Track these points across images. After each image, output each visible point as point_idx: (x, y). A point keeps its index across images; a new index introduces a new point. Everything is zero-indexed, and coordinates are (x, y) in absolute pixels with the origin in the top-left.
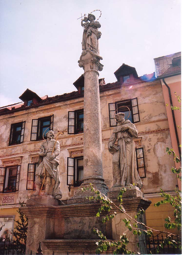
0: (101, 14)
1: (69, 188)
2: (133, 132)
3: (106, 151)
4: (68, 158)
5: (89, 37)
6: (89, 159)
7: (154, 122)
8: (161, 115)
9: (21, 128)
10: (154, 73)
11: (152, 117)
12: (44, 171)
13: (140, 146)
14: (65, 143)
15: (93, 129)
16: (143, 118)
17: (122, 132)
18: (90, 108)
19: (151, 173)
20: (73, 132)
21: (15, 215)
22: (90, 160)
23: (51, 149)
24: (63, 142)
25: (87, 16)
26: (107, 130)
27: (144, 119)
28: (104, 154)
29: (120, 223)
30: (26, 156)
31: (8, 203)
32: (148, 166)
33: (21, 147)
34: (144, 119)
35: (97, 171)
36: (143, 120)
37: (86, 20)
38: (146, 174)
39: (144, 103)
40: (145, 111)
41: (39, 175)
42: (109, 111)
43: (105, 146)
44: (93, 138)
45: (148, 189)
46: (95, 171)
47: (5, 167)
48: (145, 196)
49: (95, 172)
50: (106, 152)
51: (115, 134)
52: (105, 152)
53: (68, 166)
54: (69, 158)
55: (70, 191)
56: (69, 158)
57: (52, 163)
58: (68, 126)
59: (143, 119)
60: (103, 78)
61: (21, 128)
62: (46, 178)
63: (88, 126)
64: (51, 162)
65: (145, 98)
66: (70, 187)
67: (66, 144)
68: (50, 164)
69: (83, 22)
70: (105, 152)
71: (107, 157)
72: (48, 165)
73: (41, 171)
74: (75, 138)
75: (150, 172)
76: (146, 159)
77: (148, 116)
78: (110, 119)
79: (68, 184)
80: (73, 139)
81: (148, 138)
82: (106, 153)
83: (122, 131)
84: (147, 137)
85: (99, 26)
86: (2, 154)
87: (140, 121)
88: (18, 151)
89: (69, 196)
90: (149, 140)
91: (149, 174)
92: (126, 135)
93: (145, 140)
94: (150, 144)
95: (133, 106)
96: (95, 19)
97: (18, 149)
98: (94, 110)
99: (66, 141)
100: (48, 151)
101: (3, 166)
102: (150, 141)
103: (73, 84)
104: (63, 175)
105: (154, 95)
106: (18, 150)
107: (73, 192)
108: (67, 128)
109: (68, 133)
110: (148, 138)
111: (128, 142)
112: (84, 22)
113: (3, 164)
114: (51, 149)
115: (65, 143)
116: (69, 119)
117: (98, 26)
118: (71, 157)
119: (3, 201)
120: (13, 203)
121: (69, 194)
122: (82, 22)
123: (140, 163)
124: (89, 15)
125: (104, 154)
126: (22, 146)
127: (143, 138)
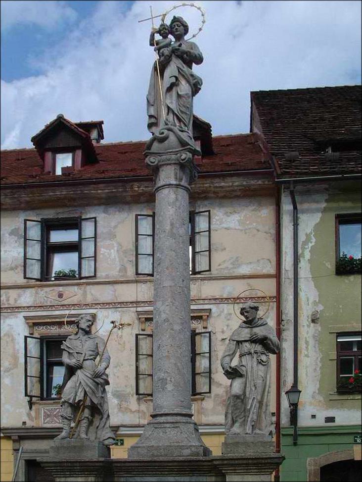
0: (204, 22)
1: (28, 402)
2: (273, 344)
4: (26, 337)
5: (174, 89)
6: (169, 379)
7: (243, 277)
8: (262, 262)
10: (191, 69)
11: (239, 266)
12: (80, 396)
13: (204, 328)
14: (16, 300)
15: (179, 321)
16: (219, 265)
17: (251, 343)
18: (174, 274)
19: (222, 386)
22: (171, 381)
23: (91, 353)
24: (9, 297)
25: (168, 22)
26: (128, 282)
27: (221, 267)
28: (117, 336)
32: (217, 372)
34: (221, 267)
35: (183, 402)
36: (217, 270)
37: (164, 31)
38: (212, 386)
39: (226, 228)
40: (225, 249)
41: (71, 401)
42: (137, 235)
44: (177, 339)
45: (212, 415)
46: (181, 401)
48: (202, 429)
49: (180, 402)
51: (235, 342)
53: (26, 356)
54: (28, 339)
55: (31, 408)
56: (28, 339)
57: (98, 381)
58: (25, 258)
59: (219, 267)
60: (96, 119)
62: (83, 411)
63: (167, 314)
64: (95, 380)
65: (229, 214)
66: (31, 400)
67: (19, 302)
68: (94, 383)
69: (156, 35)
71: (124, 343)
72: (91, 385)
73: (73, 395)
75: (221, 385)
76: (214, 357)
77: (229, 262)
78: (137, 254)
79: (26, 395)
81: (226, 312)
83: (253, 341)
84: (223, 310)
85: (199, 60)
87: (210, 270)
89: (29, 418)
90: (225, 318)
91: (218, 387)
92: (259, 348)
93: (218, 316)
94: (228, 326)
95: (197, 231)
96: (186, 30)
98: (181, 280)
99: (19, 296)
100: (86, 358)
102: (229, 320)
104: (13, 374)
105: (253, 212)
107: (38, 413)
109: (25, 277)
110: (226, 312)
111: (262, 361)
112: (158, 37)
114: (91, 353)
115: (16, 300)
116: (26, 239)
117: (192, 58)
118: (32, 334)
122: (152, 36)
123: (201, 363)
124: (175, 20)
127: (213, 311)
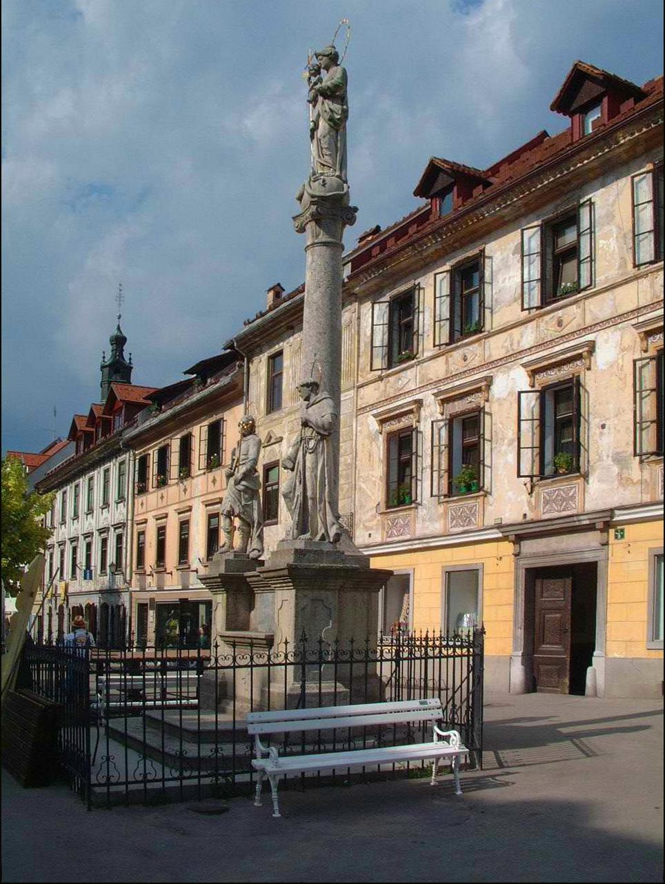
3: (625, 357)
9: (576, 261)
14: (519, 343)
20: (536, 302)
21: (413, 567)
28: (618, 367)
29: (138, 768)
30: (429, 397)
31: (398, 536)
33: (415, 368)
43: (620, 338)
47: (540, 389)
50: (623, 360)
52: (620, 361)
61: (576, 261)
67: (521, 344)
70: (620, 361)
74: (542, 322)
80: (537, 326)
82: (622, 366)
86: (377, 396)
88: (410, 383)
97: (409, 378)
101: (646, 351)
103: (552, 110)
106: (410, 380)
108: (519, 291)
113: (645, 342)
119: (387, 533)
120: (408, 537)
121: (529, 503)
125: (618, 367)
126: (419, 367)
